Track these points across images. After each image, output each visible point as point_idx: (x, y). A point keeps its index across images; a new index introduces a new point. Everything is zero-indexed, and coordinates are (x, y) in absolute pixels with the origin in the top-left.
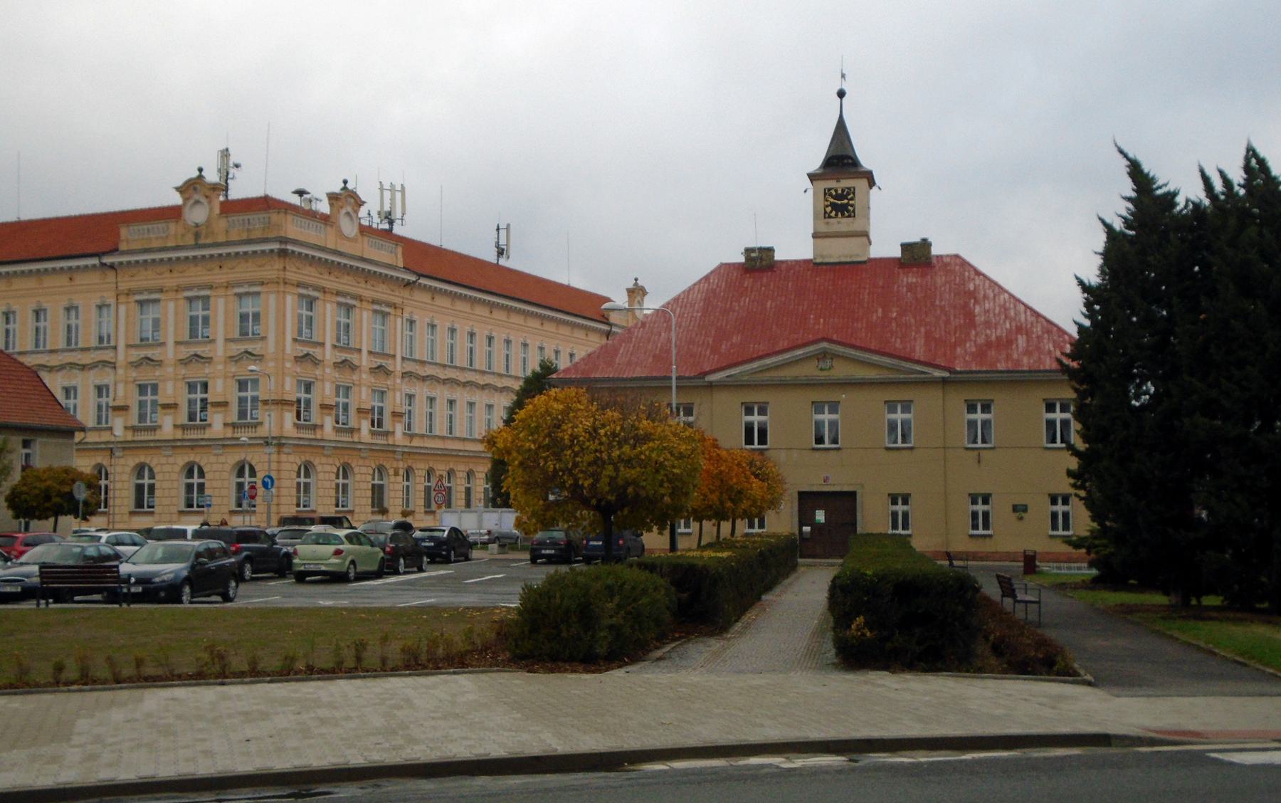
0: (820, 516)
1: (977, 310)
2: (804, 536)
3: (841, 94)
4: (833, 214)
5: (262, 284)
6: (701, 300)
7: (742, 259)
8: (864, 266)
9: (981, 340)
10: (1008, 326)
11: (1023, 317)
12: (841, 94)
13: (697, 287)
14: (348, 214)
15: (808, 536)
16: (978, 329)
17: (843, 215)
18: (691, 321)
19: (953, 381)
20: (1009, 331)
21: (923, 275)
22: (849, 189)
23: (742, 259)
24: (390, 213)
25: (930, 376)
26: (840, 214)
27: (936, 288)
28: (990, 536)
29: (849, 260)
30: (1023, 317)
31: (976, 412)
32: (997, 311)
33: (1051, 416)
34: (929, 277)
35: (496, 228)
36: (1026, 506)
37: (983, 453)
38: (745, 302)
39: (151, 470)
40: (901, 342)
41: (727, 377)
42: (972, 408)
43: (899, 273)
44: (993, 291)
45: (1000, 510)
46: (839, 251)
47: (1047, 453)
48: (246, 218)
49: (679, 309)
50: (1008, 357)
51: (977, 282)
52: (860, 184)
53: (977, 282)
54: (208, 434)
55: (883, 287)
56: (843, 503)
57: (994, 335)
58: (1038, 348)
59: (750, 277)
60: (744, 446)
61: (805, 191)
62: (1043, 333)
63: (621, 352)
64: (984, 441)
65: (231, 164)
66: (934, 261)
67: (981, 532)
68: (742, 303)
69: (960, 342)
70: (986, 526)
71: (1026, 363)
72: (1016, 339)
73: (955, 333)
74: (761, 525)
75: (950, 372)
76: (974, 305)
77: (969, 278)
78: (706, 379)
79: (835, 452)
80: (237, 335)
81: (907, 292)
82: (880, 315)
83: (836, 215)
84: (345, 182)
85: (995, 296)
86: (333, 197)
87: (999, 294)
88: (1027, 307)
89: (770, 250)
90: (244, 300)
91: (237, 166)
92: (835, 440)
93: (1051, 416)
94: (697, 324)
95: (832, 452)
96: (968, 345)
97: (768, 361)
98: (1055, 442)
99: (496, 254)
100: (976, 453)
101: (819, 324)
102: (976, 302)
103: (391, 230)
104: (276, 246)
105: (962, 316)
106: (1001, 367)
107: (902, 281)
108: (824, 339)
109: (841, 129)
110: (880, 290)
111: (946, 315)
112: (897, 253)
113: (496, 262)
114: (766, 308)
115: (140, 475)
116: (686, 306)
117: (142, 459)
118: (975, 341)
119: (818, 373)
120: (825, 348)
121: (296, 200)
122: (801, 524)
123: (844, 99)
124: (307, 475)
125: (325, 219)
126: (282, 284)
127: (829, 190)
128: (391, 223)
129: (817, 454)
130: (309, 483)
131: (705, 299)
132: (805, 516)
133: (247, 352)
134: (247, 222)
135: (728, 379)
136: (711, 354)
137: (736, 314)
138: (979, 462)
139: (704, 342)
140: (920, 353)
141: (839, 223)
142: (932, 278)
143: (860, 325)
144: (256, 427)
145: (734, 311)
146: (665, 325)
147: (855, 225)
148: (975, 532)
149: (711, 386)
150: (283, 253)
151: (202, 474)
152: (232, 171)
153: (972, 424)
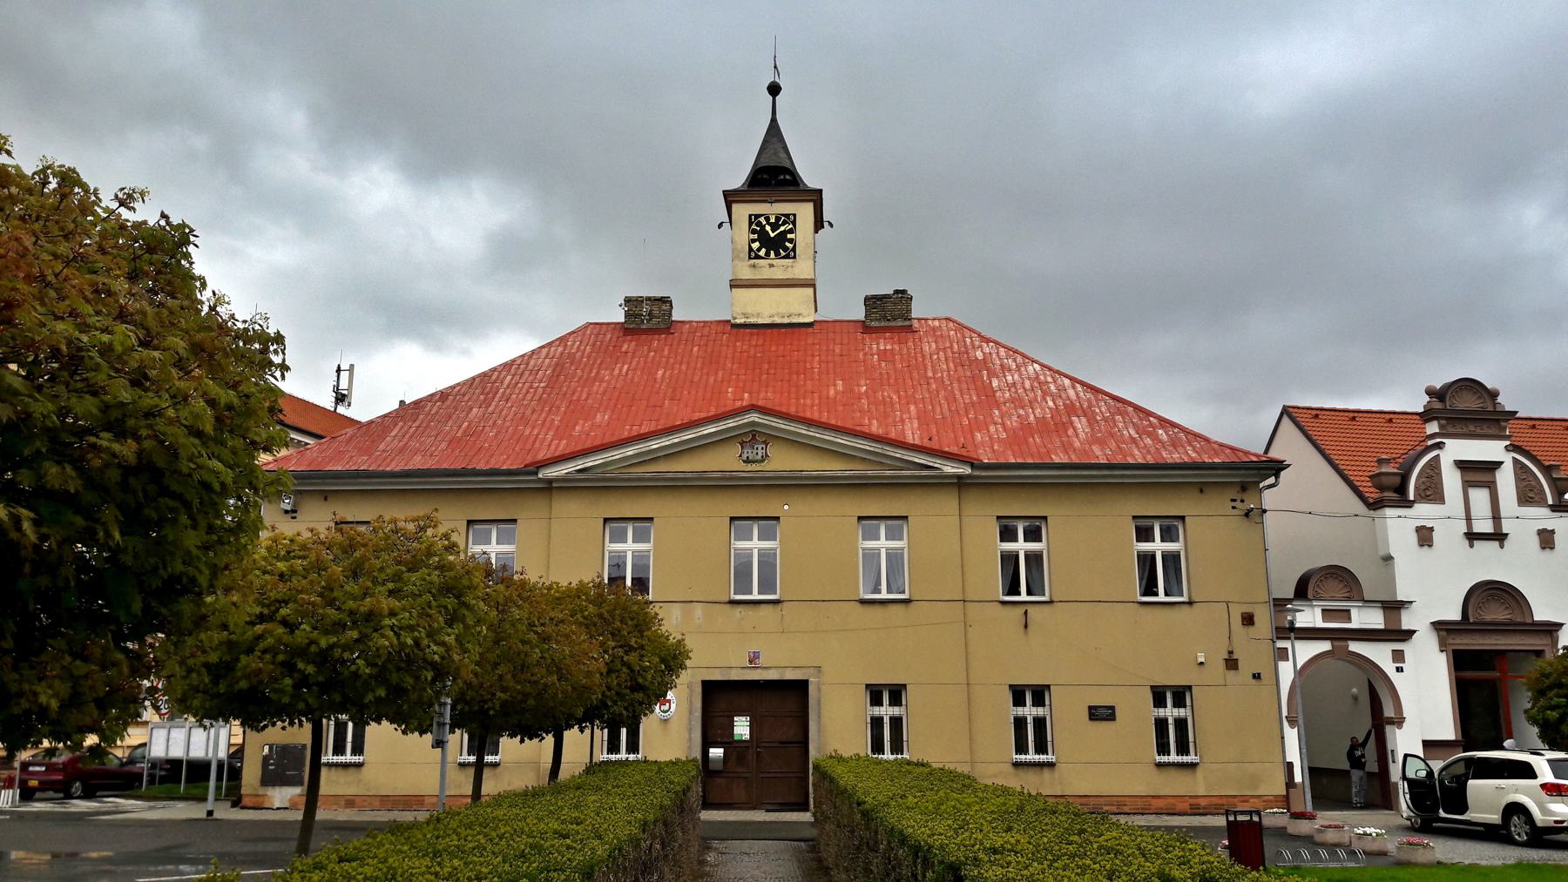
0: (742, 728)
1: (995, 383)
2: (711, 766)
3: (774, 90)
4: (763, 252)
6: (549, 366)
7: (620, 317)
8: (810, 330)
9: (1013, 422)
10: (1051, 404)
12: (774, 90)
13: (544, 351)
15: (720, 767)
17: (777, 254)
18: (528, 392)
22: (787, 216)
23: (620, 317)
26: (772, 252)
27: (923, 356)
28: (1051, 765)
29: (786, 321)
30: (1071, 392)
31: (1016, 540)
33: (1145, 546)
34: (910, 344)
35: (336, 369)
36: (1112, 708)
37: (1032, 610)
38: (621, 370)
40: (880, 425)
41: (579, 471)
44: (1015, 360)
45: (1065, 713)
49: (509, 378)
50: (1067, 447)
52: (805, 212)
57: (1032, 416)
61: (720, 226)
63: (393, 434)
66: (916, 324)
67: (1032, 756)
70: (1041, 748)
71: (1100, 455)
72: (1072, 423)
73: (967, 414)
74: (633, 747)
75: (973, 466)
76: (989, 378)
78: (540, 476)
79: (770, 607)
81: (879, 360)
83: (768, 254)
88: (1072, 379)
92: (767, 584)
93: (1145, 546)
94: (537, 397)
95: (764, 609)
97: (654, 444)
98: (1019, 594)
99: (334, 400)
100: (1020, 610)
102: (991, 374)
105: (973, 392)
107: (871, 348)
108: (753, 408)
109: (774, 131)
113: (332, 409)
116: (521, 375)
118: (1003, 424)
119: (742, 466)
120: (753, 424)
122: (707, 744)
123: (777, 98)
127: (757, 216)
129: (738, 611)
131: (557, 365)
132: (713, 728)
137: (604, 385)
138: (1026, 626)
141: (771, 266)
143: (809, 402)
146: (482, 397)
147: (801, 268)
148: (1165, 759)
149: (550, 487)
153: (1010, 560)
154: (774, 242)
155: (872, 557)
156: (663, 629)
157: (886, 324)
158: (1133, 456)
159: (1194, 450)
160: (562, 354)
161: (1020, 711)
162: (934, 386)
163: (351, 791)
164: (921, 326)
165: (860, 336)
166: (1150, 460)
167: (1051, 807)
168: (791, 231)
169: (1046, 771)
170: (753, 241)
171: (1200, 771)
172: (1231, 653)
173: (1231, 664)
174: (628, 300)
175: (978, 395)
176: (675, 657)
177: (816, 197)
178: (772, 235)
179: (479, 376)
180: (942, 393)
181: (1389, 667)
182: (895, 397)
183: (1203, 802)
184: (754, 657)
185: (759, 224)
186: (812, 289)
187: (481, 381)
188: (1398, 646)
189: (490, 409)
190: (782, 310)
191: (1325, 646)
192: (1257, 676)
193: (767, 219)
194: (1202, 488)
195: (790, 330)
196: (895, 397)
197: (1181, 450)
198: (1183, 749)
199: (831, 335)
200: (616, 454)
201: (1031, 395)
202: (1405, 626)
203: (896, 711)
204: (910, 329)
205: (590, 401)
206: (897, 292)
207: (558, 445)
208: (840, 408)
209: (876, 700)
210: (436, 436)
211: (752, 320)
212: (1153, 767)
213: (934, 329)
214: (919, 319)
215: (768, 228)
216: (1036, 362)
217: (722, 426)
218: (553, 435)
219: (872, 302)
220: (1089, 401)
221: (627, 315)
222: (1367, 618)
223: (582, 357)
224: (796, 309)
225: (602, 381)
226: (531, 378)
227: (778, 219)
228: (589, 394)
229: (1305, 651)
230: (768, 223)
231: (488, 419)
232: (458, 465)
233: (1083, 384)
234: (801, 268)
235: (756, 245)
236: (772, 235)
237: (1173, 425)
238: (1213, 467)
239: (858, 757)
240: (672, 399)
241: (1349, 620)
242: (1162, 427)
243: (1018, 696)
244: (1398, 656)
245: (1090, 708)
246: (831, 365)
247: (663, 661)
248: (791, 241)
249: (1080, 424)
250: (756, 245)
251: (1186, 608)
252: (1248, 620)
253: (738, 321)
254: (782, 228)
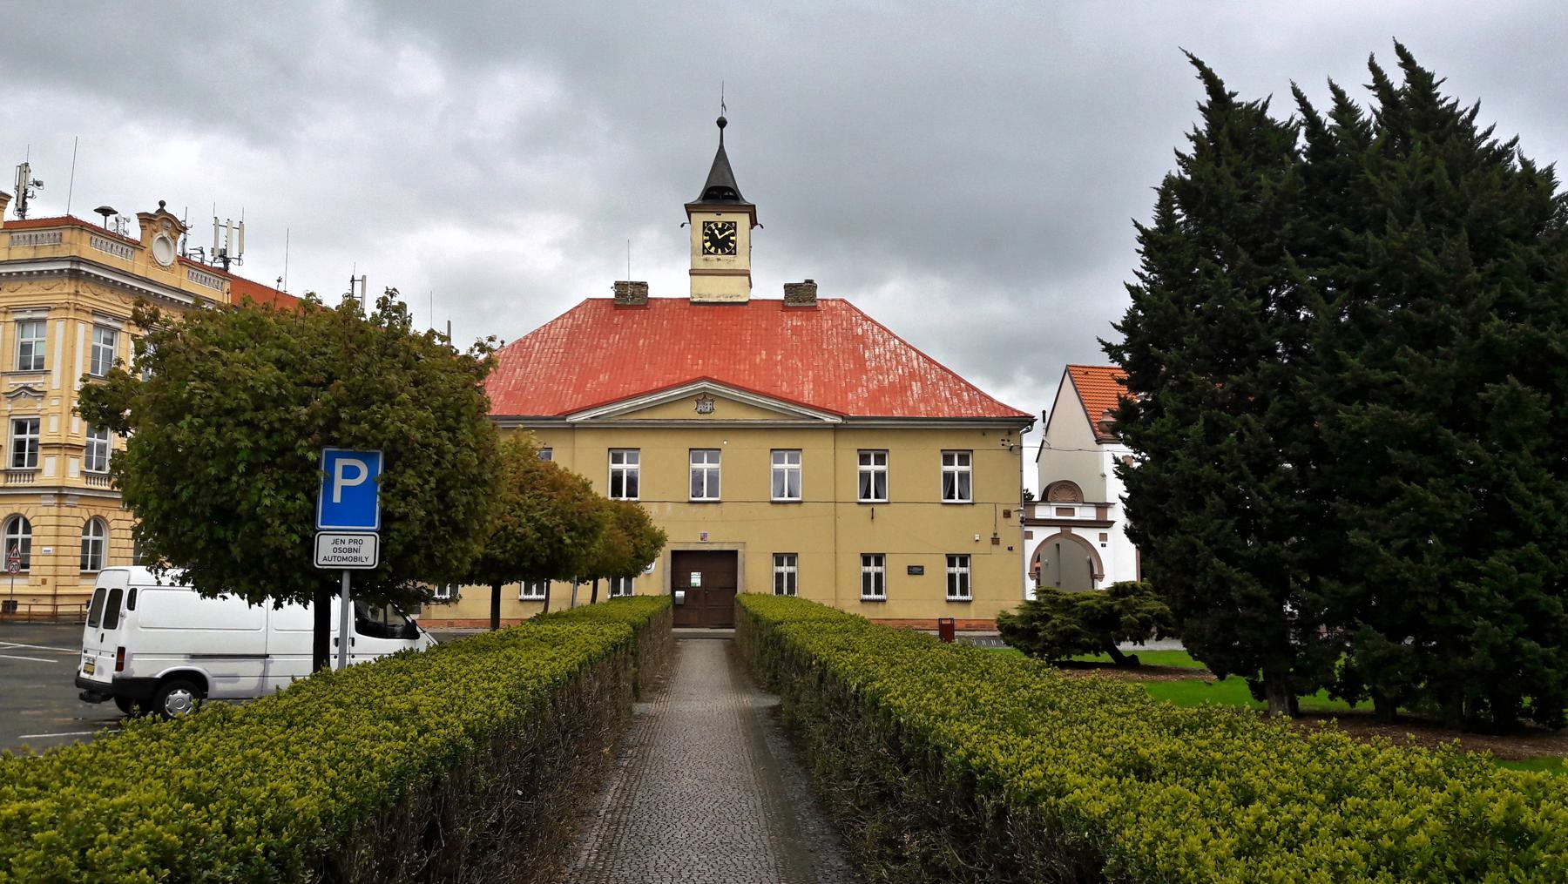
0: (696, 579)
1: (867, 355)
2: (677, 602)
3: (722, 123)
4: (713, 250)
5: (49, 309)
7: (612, 295)
8: (746, 307)
9: (874, 385)
10: (900, 371)
11: (915, 363)
12: (722, 123)
14: (163, 239)
16: (870, 375)
17: (723, 251)
19: (845, 428)
20: (902, 377)
21: (809, 319)
22: (730, 223)
23: (612, 295)
24: (225, 251)
25: (818, 422)
27: (822, 332)
28: (883, 601)
29: (729, 300)
30: (915, 363)
32: (888, 357)
33: (948, 468)
34: (814, 321)
36: (922, 567)
37: (876, 508)
39: (26, 522)
40: (788, 386)
42: (864, 459)
43: (782, 316)
44: (882, 336)
45: (893, 571)
46: (718, 290)
47: (946, 507)
48: (33, 234)
49: (538, 344)
50: (904, 405)
51: (865, 327)
52: (742, 220)
53: (865, 327)
54: (39, 481)
55: (766, 329)
56: (723, 562)
58: (934, 395)
59: (620, 315)
60: (610, 498)
61: (682, 226)
62: (938, 380)
64: (877, 496)
65: (30, 180)
66: (819, 304)
67: (873, 596)
68: (611, 341)
69: (852, 388)
71: (923, 410)
72: (911, 386)
75: (843, 418)
77: (857, 323)
79: (715, 505)
80: (16, 368)
82: (764, 356)
83: (716, 251)
84: (162, 204)
85: (884, 342)
86: (145, 219)
87: (889, 340)
88: (918, 353)
89: (643, 286)
90: (27, 328)
91: (38, 184)
93: (948, 468)
96: (860, 390)
97: (641, 401)
98: (869, 497)
100: (868, 509)
101: (698, 364)
103: (226, 268)
104: (67, 266)
105: (851, 361)
106: (897, 413)
109: (721, 155)
110: (763, 332)
111: (834, 359)
112: (781, 295)
114: (638, 347)
115: (13, 529)
116: (546, 342)
117: (98, 511)
118: (867, 387)
120: (705, 388)
121: (98, 220)
122: (674, 589)
124: (98, 532)
125: (135, 245)
126: (72, 310)
127: (709, 223)
128: (226, 261)
129: (694, 508)
130: (101, 541)
133: (26, 388)
134: (33, 238)
135: (593, 421)
136: (574, 393)
139: (566, 379)
140: (808, 397)
141: (719, 260)
142: (817, 321)
143: (742, 367)
144: (33, 475)
145: (602, 348)
147: (738, 262)
148: (952, 598)
149: (573, 428)
150: (75, 275)
151: (27, 528)
152: (31, 189)
153: (865, 476)
154: (720, 242)
155: (779, 475)
156: (653, 525)
157: (797, 304)
158: (943, 411)
159: (982, 408)
160: (572, 325)
161: (952, 570)
162: (826, 356)
163: (451, 616)
164: (823, 306)
165: (780, 313)
166: (953, 414)
167: (882, 624)
168: (733, 235)
169: (880, 604)
170: (706, 241)
171: (972, 604)
172: (995, 534)
173: (995, 541)
174: (617, 284)
175: (855, 365)
176: (659, 540)
177: (751, 211)
178: (720, 237)
179: (517, 342)
180: (832, 362)
181: (1096, 543)
182: (800, 365)
183: (974, 624)
184: (704, 537)
185: (710, 229)
186: (747, 278)
187: (519, 347)
188: (1103, 531)
189: (529, 369)
190: (726, 292)
191: (1057, 530)
192: (1010, 549)
193: (716, 225)
194: (984, 432)
195: (732, 307)
196: (800, 365)
197: (974, 408)
198: (964, 592)
199: (760, 312)
200: (617, 407)
201: (889, 364)
202: (1109, 519)
203: (791, 569)
204: (815, 309)
205: (595, 365)
206: (807, 281)
207: (576, 399)
208: (763, 373)
209: (779, 563)
210: (496, 390)
211: (705, 299)
212: (945, 604)
213: (832, 309)
214: (822, 300)
215: (716, 232)
216: (897, 338)
217: (684, 390)
218: (573, 391)
219: (789, 288)
220: (925, 369)
221: (616, 294)
222: (1086, 513)
223: (586, 328)
224: (735, 291)
225: (602, 348)
226: (553, 345)
227: (723, 225)
228: (593, 359)
229: (1041, 534)
230: (717, 228)
231: (527, 378)
232: (514, 413)
233: (924, 356)
234: (738, 262)
235: (708, 245)
236: (720, 237)
237: (974, 389)
238: (991, 420)
239: (766, 595)
240: (650, 364)
241: (1073, 515)
242: (967, 390)
243: (866, 560)
244: (1103, 537)
245: (909, 567)
246: (759, 338)
247: (653, 542)
248: (733, 242)
249: (916, 387)
250: (708, 245)
251: (970, 506)
252: (1007, 514)
253: (695, 300)
254: (727, 233)
